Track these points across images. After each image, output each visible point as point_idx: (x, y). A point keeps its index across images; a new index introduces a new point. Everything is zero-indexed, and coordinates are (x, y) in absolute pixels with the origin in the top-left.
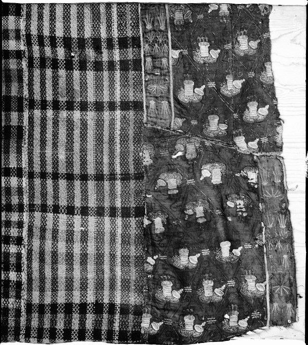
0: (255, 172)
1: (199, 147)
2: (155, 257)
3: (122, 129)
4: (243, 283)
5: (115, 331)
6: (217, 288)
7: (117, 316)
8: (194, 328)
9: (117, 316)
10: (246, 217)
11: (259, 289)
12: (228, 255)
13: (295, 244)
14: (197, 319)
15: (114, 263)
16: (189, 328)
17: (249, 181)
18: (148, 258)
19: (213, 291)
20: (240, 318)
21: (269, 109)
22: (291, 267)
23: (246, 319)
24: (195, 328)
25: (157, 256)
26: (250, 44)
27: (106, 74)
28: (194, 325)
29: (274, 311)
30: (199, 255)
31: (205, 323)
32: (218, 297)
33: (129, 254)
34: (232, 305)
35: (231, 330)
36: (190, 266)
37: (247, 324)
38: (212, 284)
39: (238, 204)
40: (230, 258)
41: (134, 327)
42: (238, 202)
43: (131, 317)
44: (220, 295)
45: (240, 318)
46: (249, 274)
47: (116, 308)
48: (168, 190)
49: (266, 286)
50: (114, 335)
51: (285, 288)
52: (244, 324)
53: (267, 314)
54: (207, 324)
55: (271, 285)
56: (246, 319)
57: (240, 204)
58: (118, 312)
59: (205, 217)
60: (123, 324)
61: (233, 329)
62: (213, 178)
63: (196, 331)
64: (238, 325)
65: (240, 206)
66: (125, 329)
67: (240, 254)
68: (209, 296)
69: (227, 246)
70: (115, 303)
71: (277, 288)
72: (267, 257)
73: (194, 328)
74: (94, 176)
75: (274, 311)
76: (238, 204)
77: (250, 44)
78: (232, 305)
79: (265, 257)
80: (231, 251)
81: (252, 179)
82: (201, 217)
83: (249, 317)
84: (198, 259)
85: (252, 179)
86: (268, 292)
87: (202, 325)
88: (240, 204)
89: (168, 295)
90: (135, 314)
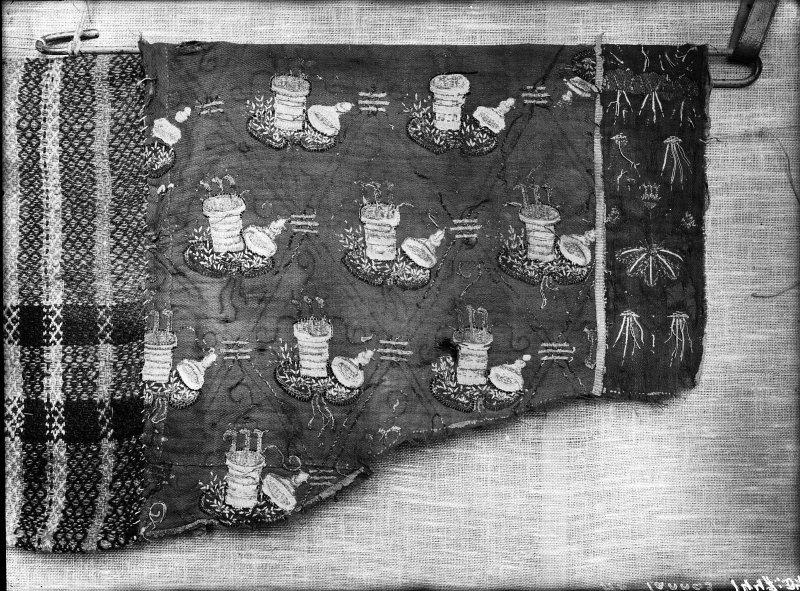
2: (182, 116)
3: (88, 243)
4: (512, 230)
5: (49, 405)
6: (413, 236)
7: (54, 353)
9: (59, 450)
11: (567, 255)
12: (455, 126)
15: (35, 162)
16: (312, 366)
18: (156, 122)
19: (399, 244)
20: (497, 356)
21: (524, 372)
23: (519, 365)
25: (188, 110)
27: (55, 297)
28: (331, 358)
29: (623, 337)
30: (347, 106)
31: (370, 353)
32: (414, 272)
33: (89, 126)
34: (469, 308)
35: (463, 399)
36: (309, 139)
37: (520, 380)
38: (395, 220)
40: (460, 136)
41: (119, 383)
43: (106, 351)
45: (497, 356)
46: (532, 202)
47: (48, 321)
49: (592, 246)
50: (51, 421)
51: (665, 255)
52: (509, 379)
53: (595, 353)
54: (375, 362)
56: (519, 365)
58: (58, 336)
60: (80, 376)
61: (470, 398)
63: (336, 381)
64: (489, 383)
66: (85, 397)
68: (381, 258)
69: (455, 91)
70: (41, 307)
71: (634, 256)
72: (603, 142)
74: (20, 435)
78: (469, 308)
79: (597, 142)
80: (467, 111)
83: (527, 357)
86: (600, 269)
87: (356, 362)
90: (116, 340)
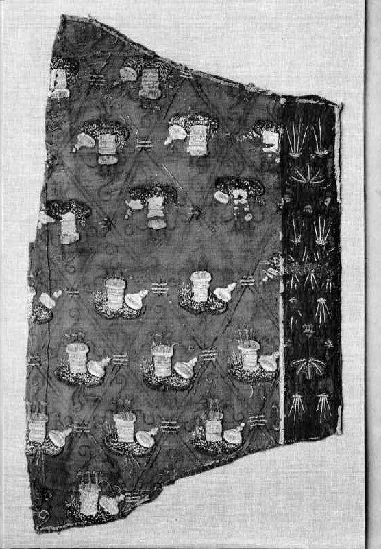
0: (278, 132)
1: (168, 80)
8: (135, 439)
10: (249, 222)
13: (345, 279)
14: (141, 420)
17: (265, 150)
20: (225, 426)
22: (330, 322)
23: (240, 429)
24: (138, 438)
26: (185, 135)
32: (181, 381)
39: (236, 196)
42: (236, 193)
44: (185, 376)
45: (225, 426)
48: (99, 155)
49: (277, 360)
51: (316, 363)
55: (288, 359)
57: (240, 197)
59: (165, 219)
62: (191, 142)
63: (138, 444)
64: (223, 440)
65: (240, 201)
67: (229, 298)
69: (203, 280)
71: (300, 364)
72: (284, 303)
73: (135, 439)
75: (293, 409)
76: (236, 196)
77: (185, 135)
81: (269, 146)
82: (156, 218)
84: (143, 300)
85: (269, 146)
88: (240, 197)
89: (81, 372)
